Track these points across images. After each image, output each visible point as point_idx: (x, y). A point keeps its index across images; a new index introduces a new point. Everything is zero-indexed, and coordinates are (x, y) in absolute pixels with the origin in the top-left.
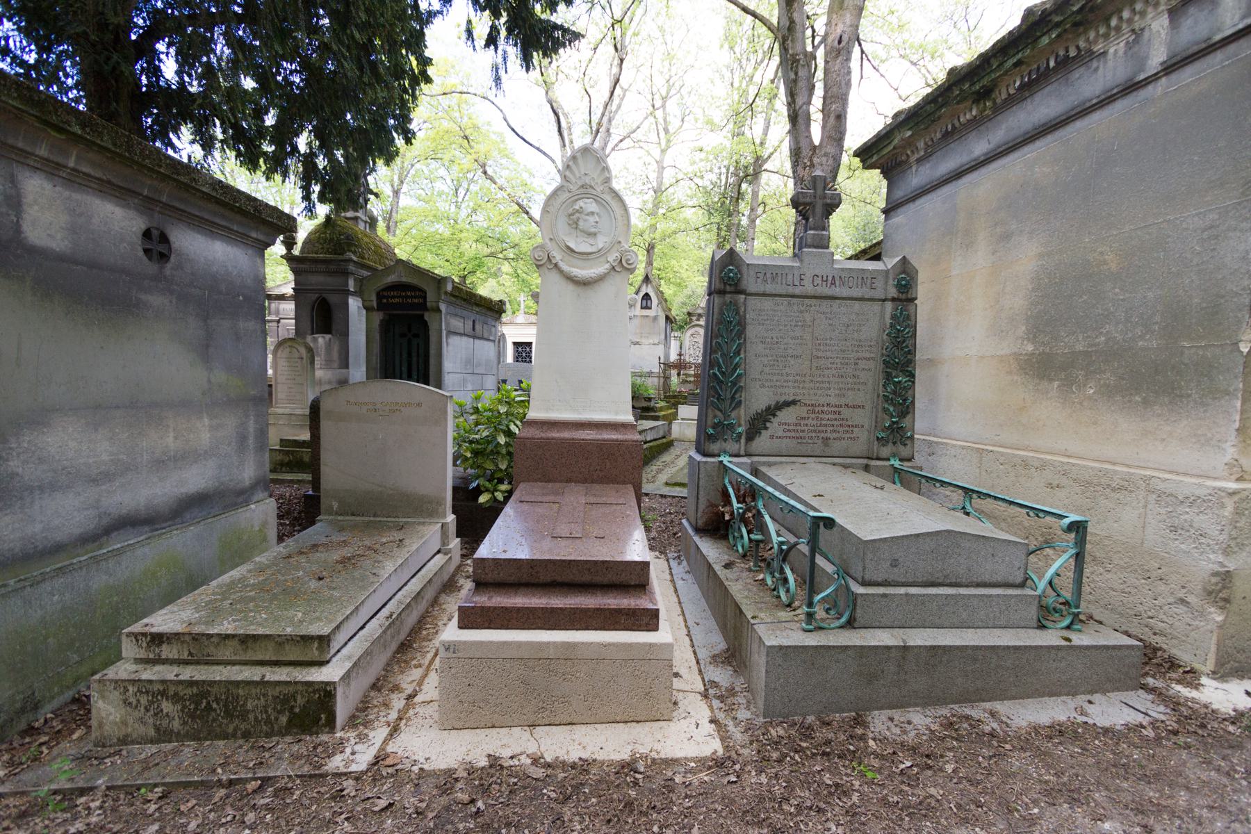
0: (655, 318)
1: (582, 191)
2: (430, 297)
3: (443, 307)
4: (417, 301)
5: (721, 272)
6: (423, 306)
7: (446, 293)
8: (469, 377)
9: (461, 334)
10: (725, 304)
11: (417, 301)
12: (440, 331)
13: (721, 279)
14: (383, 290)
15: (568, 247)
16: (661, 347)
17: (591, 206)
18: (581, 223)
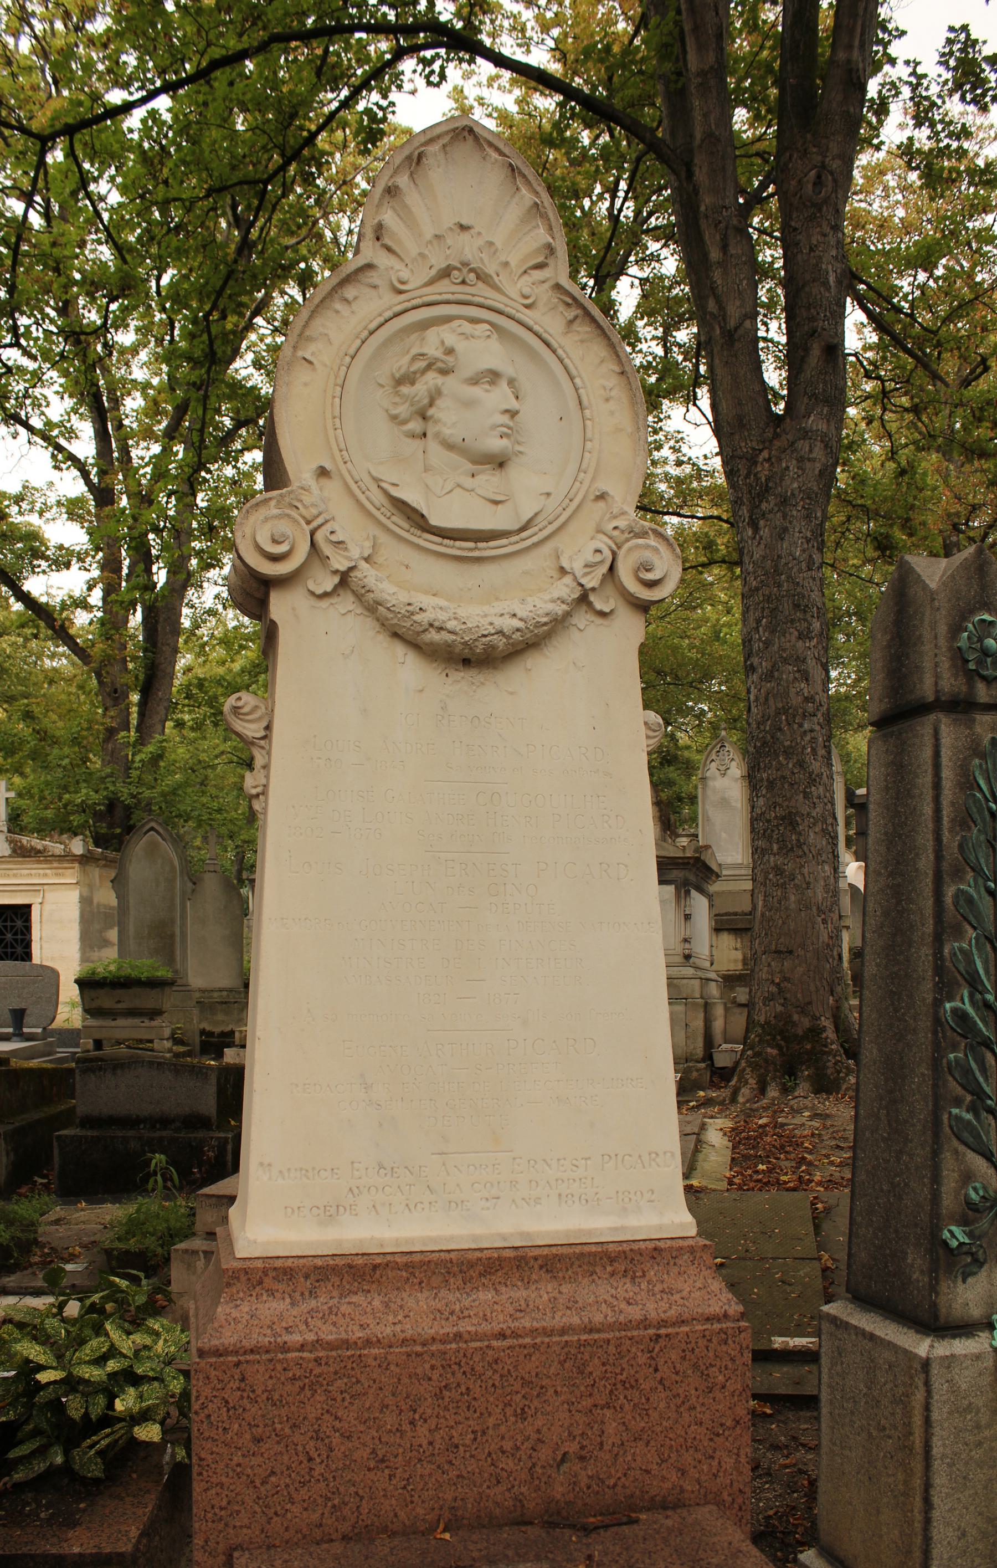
1: (445, 288)
5: (956, 630)
10: (976, 750)
13: (959, 657)
15: (401, 506)
18: (449, 418)
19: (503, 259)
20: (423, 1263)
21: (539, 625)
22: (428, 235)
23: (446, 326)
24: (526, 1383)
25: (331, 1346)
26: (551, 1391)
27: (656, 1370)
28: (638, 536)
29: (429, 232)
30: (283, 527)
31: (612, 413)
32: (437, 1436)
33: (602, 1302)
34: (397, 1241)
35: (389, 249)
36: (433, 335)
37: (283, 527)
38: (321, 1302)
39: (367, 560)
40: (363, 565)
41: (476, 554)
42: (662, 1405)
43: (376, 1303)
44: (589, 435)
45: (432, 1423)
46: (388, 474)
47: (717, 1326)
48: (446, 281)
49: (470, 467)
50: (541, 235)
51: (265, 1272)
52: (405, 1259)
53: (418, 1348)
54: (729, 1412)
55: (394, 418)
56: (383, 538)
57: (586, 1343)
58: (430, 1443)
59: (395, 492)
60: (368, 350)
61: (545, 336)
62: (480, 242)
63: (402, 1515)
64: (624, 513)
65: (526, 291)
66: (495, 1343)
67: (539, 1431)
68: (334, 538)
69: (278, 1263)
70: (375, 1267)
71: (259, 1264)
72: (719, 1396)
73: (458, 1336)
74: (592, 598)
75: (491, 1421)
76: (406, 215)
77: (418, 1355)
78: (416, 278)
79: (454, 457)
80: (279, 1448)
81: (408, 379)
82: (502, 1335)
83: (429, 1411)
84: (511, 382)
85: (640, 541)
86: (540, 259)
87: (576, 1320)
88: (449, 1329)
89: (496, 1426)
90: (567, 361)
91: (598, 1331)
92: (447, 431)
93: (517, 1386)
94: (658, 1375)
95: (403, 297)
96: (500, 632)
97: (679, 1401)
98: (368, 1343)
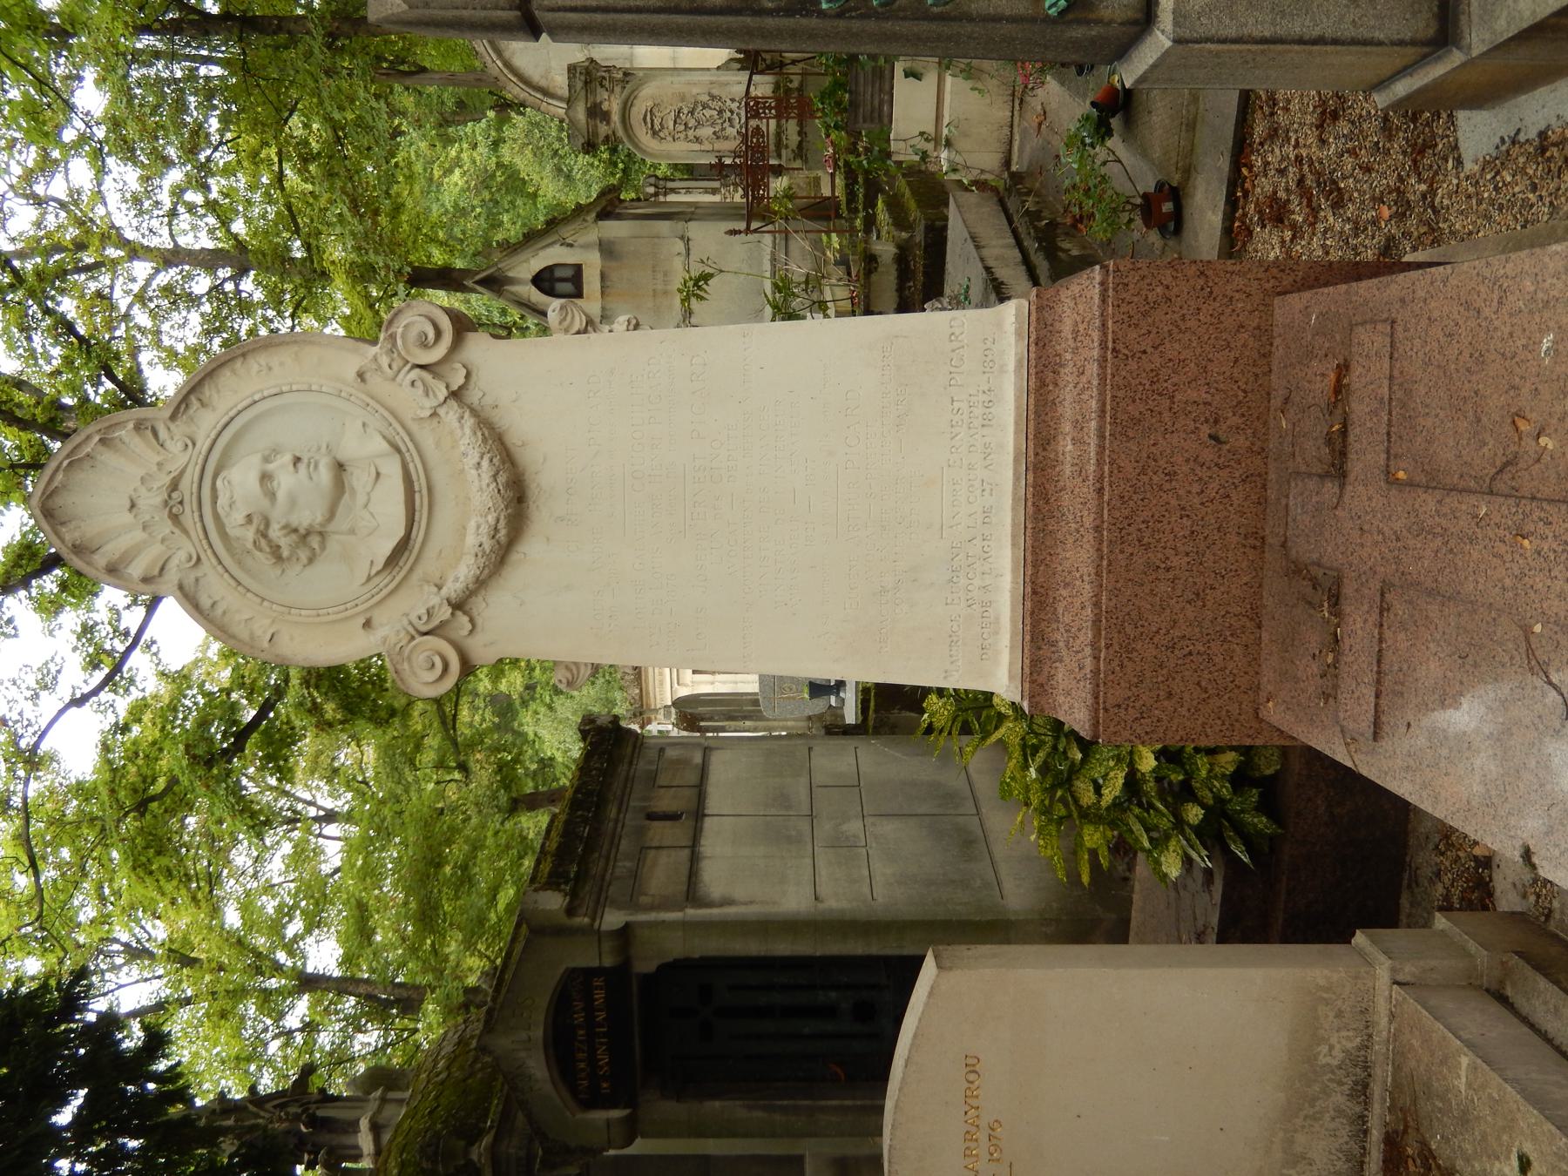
0: (607, 249)
1: (189, 518)
2: (586, 957)
3: (613, 919)
4: (599, 996)
6: (619, 976)
7: (570, 911)
8: (825, 828)
9: (695, 858)
11: (599, 996)
12: (686, 925)
14: (574, 1090)
16: (695, 229)
17: (241, 480)
18: (307, 516)
19: (155, 468)
20: (1034, 553)
21: (485, 440)
22: (144, 535)
23: (225, 520)
24: (1143, 472)
25: (1097, 634)
26: (1153, 449)
27: (1145, 352)
28: (394, 344)
29: (138, 535)
30: (420, 659)
31: (282, 364)
32: (1181, 549)
33: (1079, 398)
34: (1014, 570)
35: (162, 569)
36: (233, 532)
37: (420, 659)
38: (1060, 637)
39: (439, 587)
40: (444, 591)
41: (425, 492)
42: (1176, 346)
43: (1064, 593)
44: (305, 387)
45: (1169, 552)
46: (362, 572)
47: (1111, 292)
48: (182, 518)
49: (347, 496)
50: (125, 433)
51: (1032, 682)
52: (1029, 567)
53: (1105, 563)
54: (1192, 282)
55: (311, 561)
56: (415, 577)
57: (1114, 417)
58: (1187, 554)
59: (379, 565)
60: (254, 586)
61: (219, 427)
62: (143, 491)
63: (1245, 579)
64: (375, 359)
65: (180, 445)
66: (1106, 498)
67: (1188, 460)
68: (425, 618)
69: (1027, 670)
70: (1034, 592)
71: (1027, 685)
72: (1175, 290)
73: (1098, 529)
74: (455, 387)
75: (1174, 502)
76: (128, 557)
77: (1109, 565)
78: (184, 549)
79: (341, 510)
80: (1178, 677)
81: (276, 551)
82: (1100, 491)
83: (1160, 555)
84: (267, 460)
85: (399, 342)
86: (149, 433)
87: (1093, 424)
88: (1090, 537)
89: (1179, 497)
90: (240, 407)
91: (1104, 404)
92: (319, 519)
93: (1145, 479)
94: (1149, 350)
95: (203, 557)
96: (495, 477)
97: (1176, 330)
98: (1097, 605)
